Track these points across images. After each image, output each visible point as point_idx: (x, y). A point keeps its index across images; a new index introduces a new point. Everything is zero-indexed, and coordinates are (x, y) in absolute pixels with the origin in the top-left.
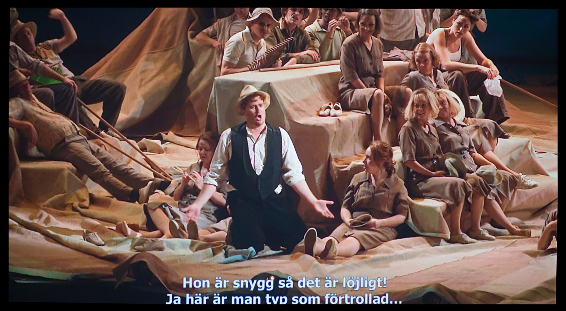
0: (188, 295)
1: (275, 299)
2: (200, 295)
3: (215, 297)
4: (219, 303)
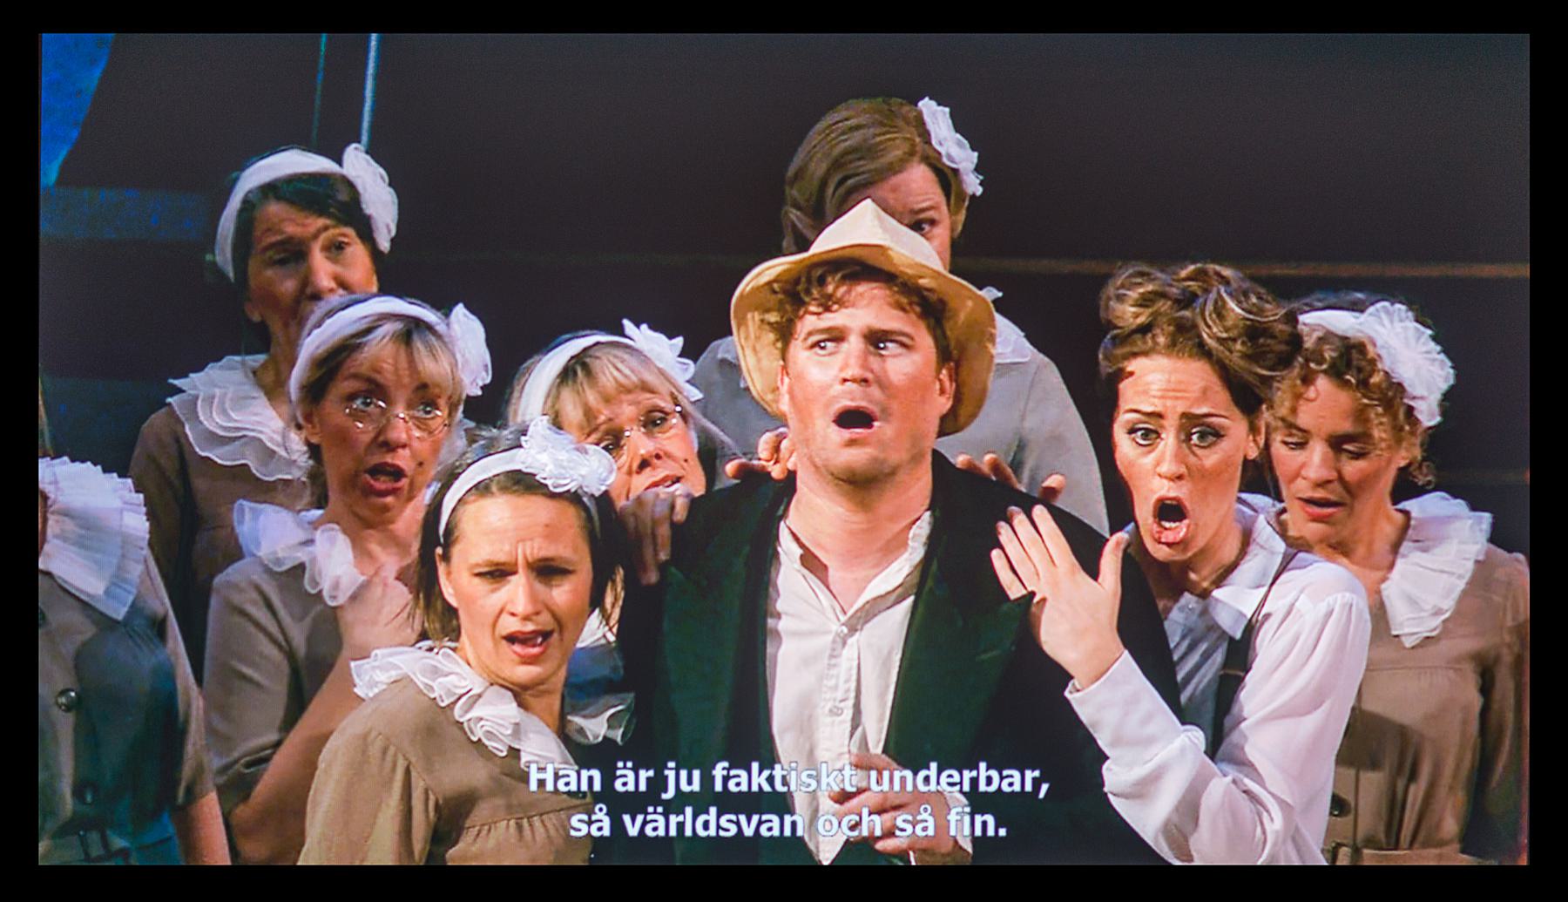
3: (619, 773)
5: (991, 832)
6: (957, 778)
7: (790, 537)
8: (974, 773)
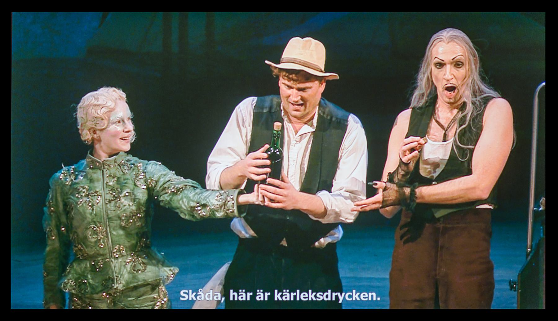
0: (232, 291)
1: (278, 294)
2: (288, 291)
3: (258, 294)
4: (288, 299)
5: (374, 299)
6: (367, 296)
7: (235, 122)
8: (295, 294)
